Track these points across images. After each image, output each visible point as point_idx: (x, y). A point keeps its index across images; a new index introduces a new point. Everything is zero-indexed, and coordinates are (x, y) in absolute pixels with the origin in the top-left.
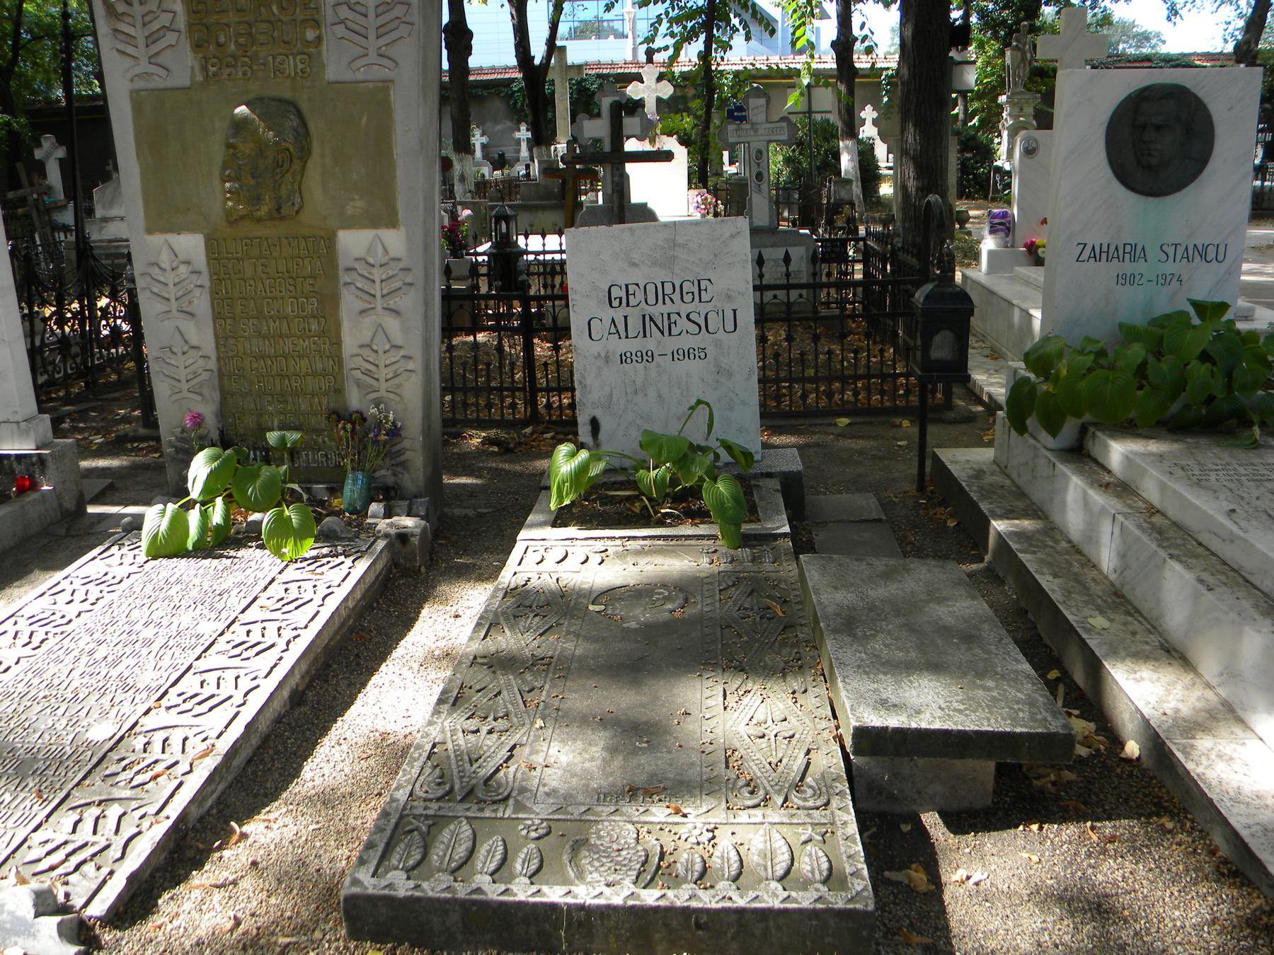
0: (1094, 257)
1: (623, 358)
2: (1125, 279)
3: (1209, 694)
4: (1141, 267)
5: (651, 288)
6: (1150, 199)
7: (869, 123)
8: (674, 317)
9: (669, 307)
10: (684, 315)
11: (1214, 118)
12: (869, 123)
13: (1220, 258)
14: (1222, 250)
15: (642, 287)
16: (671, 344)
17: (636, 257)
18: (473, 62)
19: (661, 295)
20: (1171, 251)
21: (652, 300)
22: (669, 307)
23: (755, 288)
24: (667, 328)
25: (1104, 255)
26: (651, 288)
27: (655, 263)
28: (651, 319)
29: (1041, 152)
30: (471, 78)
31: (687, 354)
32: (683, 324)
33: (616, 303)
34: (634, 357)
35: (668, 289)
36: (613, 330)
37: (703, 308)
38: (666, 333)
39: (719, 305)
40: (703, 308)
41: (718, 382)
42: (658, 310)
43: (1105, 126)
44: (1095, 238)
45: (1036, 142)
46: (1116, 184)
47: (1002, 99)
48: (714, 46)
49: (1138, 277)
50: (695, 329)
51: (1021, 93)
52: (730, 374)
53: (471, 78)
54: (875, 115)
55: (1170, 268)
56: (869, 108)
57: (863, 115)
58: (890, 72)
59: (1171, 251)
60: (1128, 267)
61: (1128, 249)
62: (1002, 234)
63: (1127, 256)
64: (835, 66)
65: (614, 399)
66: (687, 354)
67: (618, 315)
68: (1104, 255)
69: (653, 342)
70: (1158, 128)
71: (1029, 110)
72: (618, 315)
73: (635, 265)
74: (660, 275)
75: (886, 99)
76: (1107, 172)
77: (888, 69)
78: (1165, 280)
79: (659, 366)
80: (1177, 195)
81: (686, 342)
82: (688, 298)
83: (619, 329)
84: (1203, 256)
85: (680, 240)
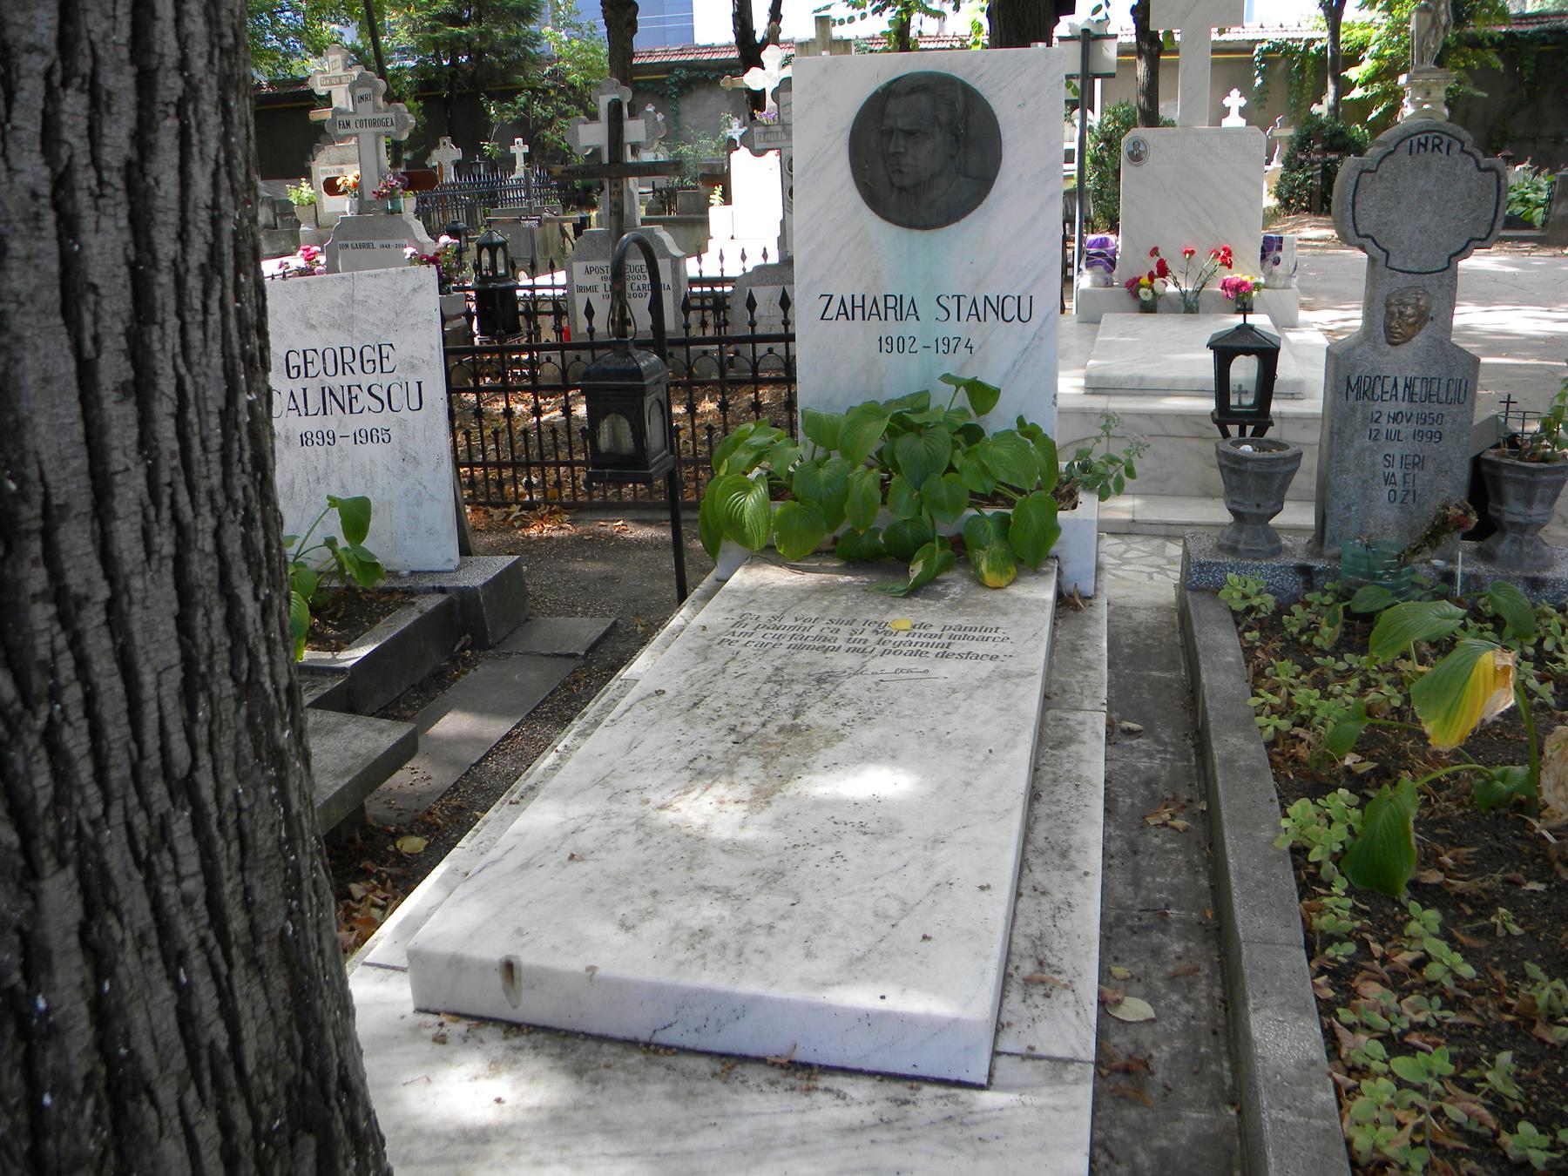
0: (846, 312)
2: (891, 345)
3: (262, 856)
4: (910, 327)
5: (329, 355)
6: (917, 232)
7: (1234, 112)
8: (355, 390)
10: (365, 389)
11: (1000, 119)
12: (1234, 112)
13: (1025, 316)
16: (354, 423)
17: (314, 317)
18: (640, 43)
19: (341, 366)
21: (331, 370)
23: (792, 338)
24: (348, 407)
25: (858, 311)
26: (329, 355)
27: (333, 325)
28: (331, 393)
30: (635, 62)
31: (370, 436)
32: (364, 399)
33: (294, 373)
35: (348, 357)
36: (292, 406)
37: (386, 380)
39: (402, 376)
40: (386, 380)
41: (403, 470)
42: (337, 382)
43: (848, 133)
44: (843, 288)
46: (867, 213)
47: (1402, 79)
49: (908, 342)
50: (376, 405)
51: (1429, 71)
52: (417, 463)
53: (635, 62)
54: (1243, 102)
55: (953, 329)
56: (1235, 93)
58: (1265, 45)
60: (893, 328)
62: (1101, 269)
63: (891, 313)
64: (1134, 39)
65: (297, 489)
66: (370, 436)
68: (858, 311)
69: (333, 421)
70: (909, 134)
71: (1441, 94)
73: (312, 327)
74: (339, 339)
75: (1259, 81)
76: (853, 196)
77: (1263, 41)
78: (948, 346)
79: (341, 450)
80: (954, 227)
81: (369, 421)
82: (369, 367)
84: (1000, 312)
85: (359, 296)
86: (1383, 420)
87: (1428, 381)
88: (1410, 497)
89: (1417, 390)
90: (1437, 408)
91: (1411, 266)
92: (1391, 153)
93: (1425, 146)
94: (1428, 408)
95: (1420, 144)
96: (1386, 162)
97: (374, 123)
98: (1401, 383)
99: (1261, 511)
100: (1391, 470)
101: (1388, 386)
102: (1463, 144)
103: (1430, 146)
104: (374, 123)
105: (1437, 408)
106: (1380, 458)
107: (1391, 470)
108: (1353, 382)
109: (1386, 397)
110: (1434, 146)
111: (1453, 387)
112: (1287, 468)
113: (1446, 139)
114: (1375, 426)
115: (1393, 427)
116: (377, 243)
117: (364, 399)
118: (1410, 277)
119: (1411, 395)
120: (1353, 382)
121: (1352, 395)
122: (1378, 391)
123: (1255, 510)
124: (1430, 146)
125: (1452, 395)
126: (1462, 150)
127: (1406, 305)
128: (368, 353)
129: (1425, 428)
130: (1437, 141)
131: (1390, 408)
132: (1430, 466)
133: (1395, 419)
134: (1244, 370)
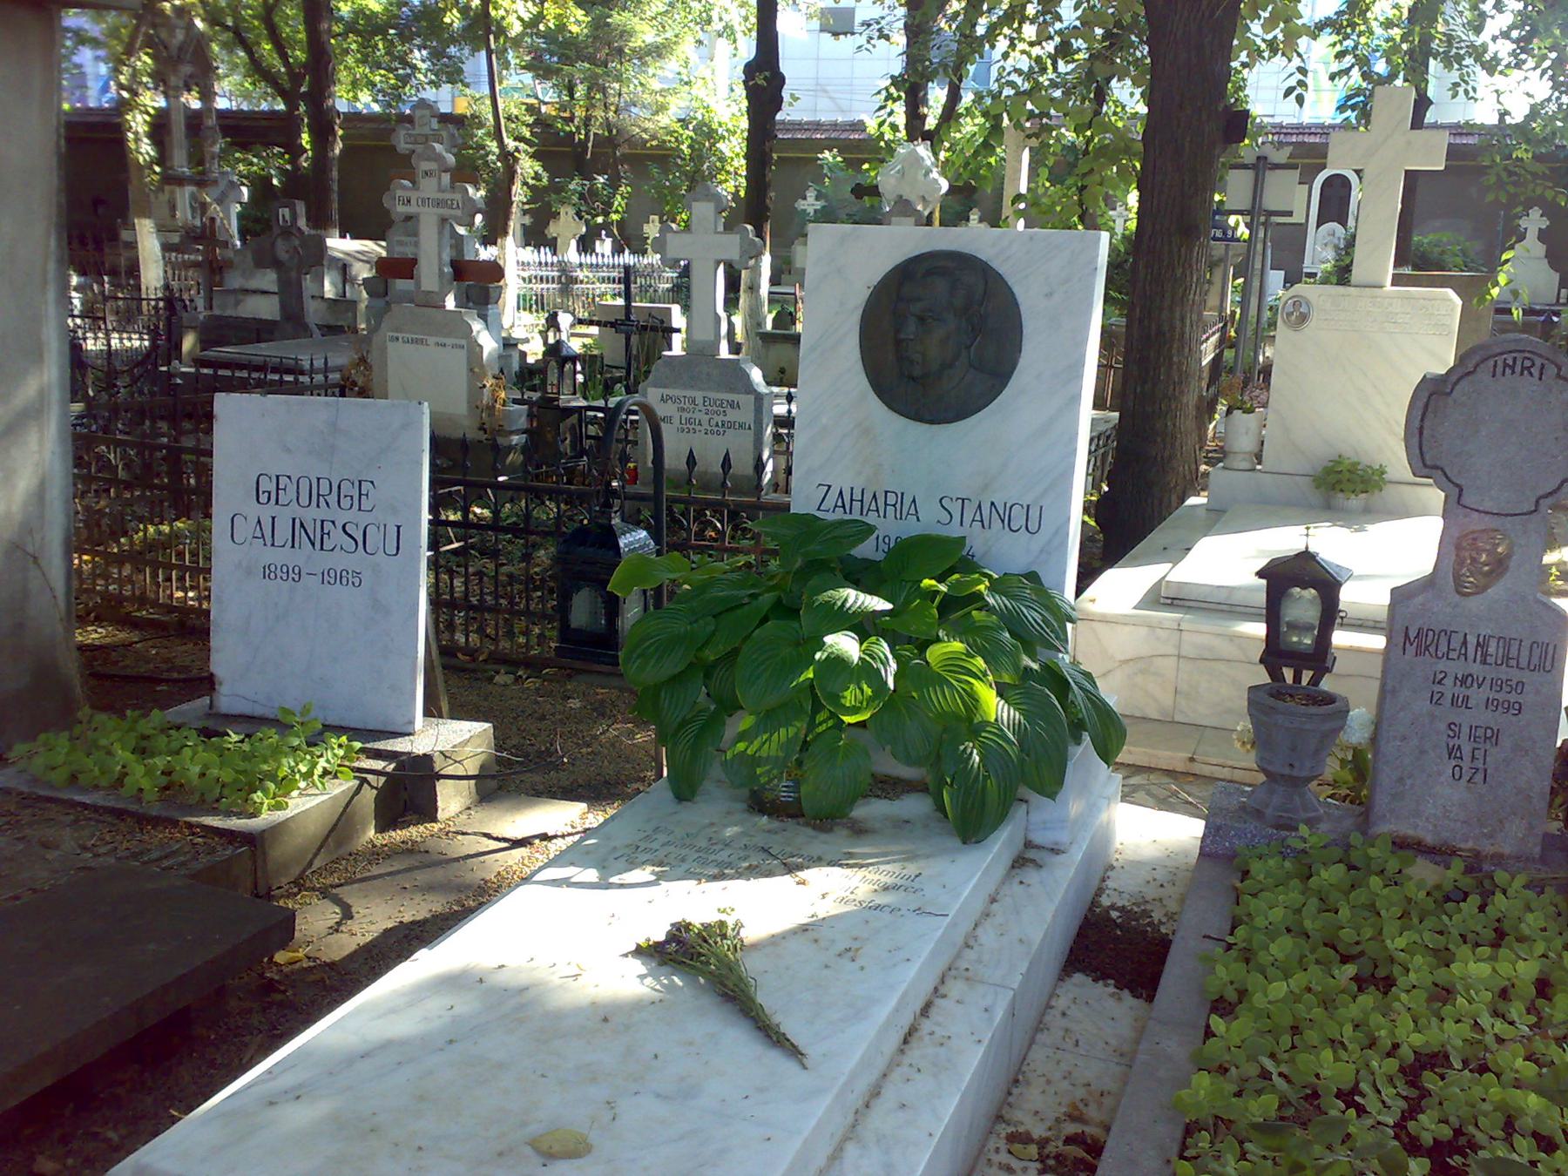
1: (268, 572)
7: (1532, 235)
9: (323, 513)
10: (339, 526)
12: (1532, 235)
13: (1033, 526)
14: (1034, 513)
15: (294, 480)
19: (316, 498)
20: (955, 508)
21: (304, 500)
22: (323, 513)
24: (319, 541)
28: (302, 525)
29: (1313, 323)
31: (340, 577)
32: (337, 536)
33: (263, 498)
34: (279, 574)
35: (324, 490)
37: (364, 518)
38: (318, 545)
40: (364, 518)
42: (311, 515)
45: (1308, 304)
48: (1148, 61)
54: (1544, 223)
57: (1523, 223)
59: (955, 508)
61: (891, 499)
66: (340, 577)
67: (265, 514)
69: (303, 555)
72: (265, 514)
73: (288, 450)
74: (316, 469)
81: (339, 561)
82: (346, 503)
83: (265, 534)
86: (1449, 682)
87: (1506, 642)
88: (1480, 776)
89: (1492, 650)
90: (1516, 675)
91: (1487, 505)
92: (1469, 373)
93: (1513, 368)
94: (1503, 673)
95: (1506, 365)
96: (1464, 383)
97: (439, 203)
98: (1472, 640)
99: (1295, 773)
100: (1456, 741)
101: (1456, 644)
102: (1559, 369)
103: (1518, 369)
104: (439, 203)
105: (1516, 675)
106: (1443, 726)
107: (1456, 741)
108: (1412, 635)
109: (1453, 655)
110: (1523, 368)
111: (1536, 652)
112: (1327, 726)
113: (1538, 362)
114: (1437, 688)
115: (1460, 691)
116: (432, 340)
117: (337, 536)
118: (1487, 518)
119: (1485, 655)
120: (1412, 635)
121: (1411, 650)
122: (1443, 648)
123: (1287, 771)
124: (1518, 369)
125: (1535, 660)
126: (1558, 376)
127: (1479, 551)
128: (345, 486)
129: (1501, 696)
130: (1527, 363)
131: (1457, 668)
132: (1506, 742)
133: (1463, 682)
134: (1303, 605)
